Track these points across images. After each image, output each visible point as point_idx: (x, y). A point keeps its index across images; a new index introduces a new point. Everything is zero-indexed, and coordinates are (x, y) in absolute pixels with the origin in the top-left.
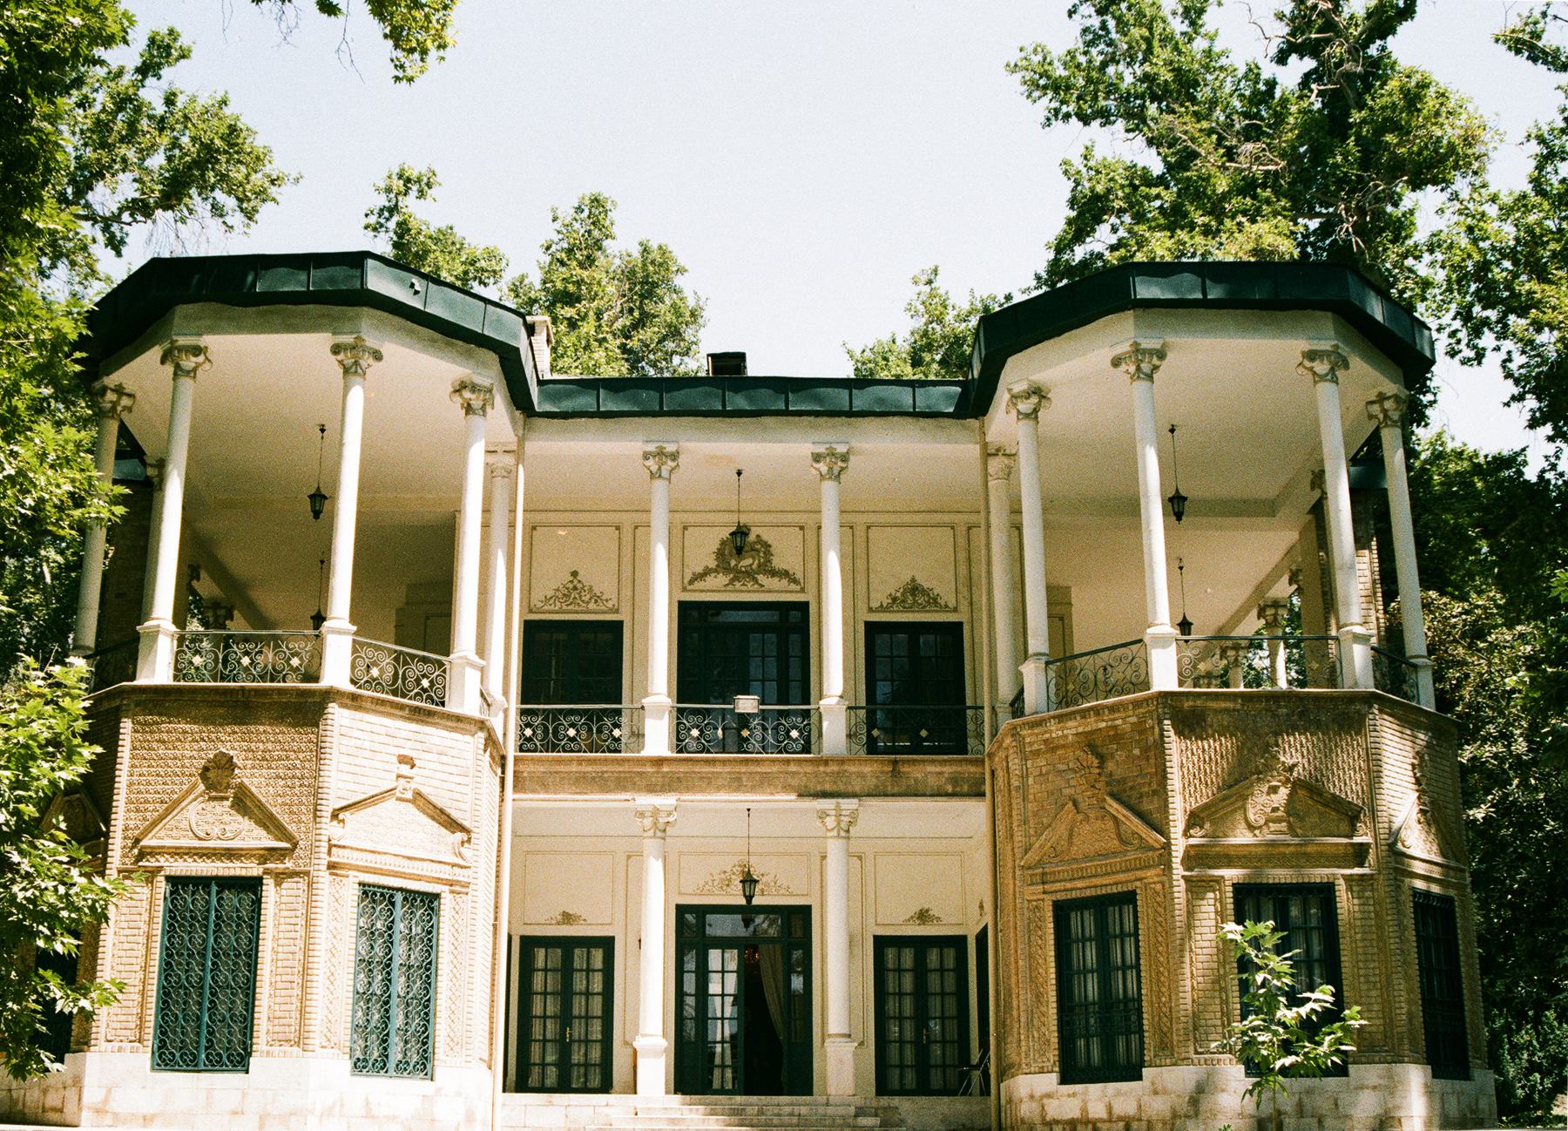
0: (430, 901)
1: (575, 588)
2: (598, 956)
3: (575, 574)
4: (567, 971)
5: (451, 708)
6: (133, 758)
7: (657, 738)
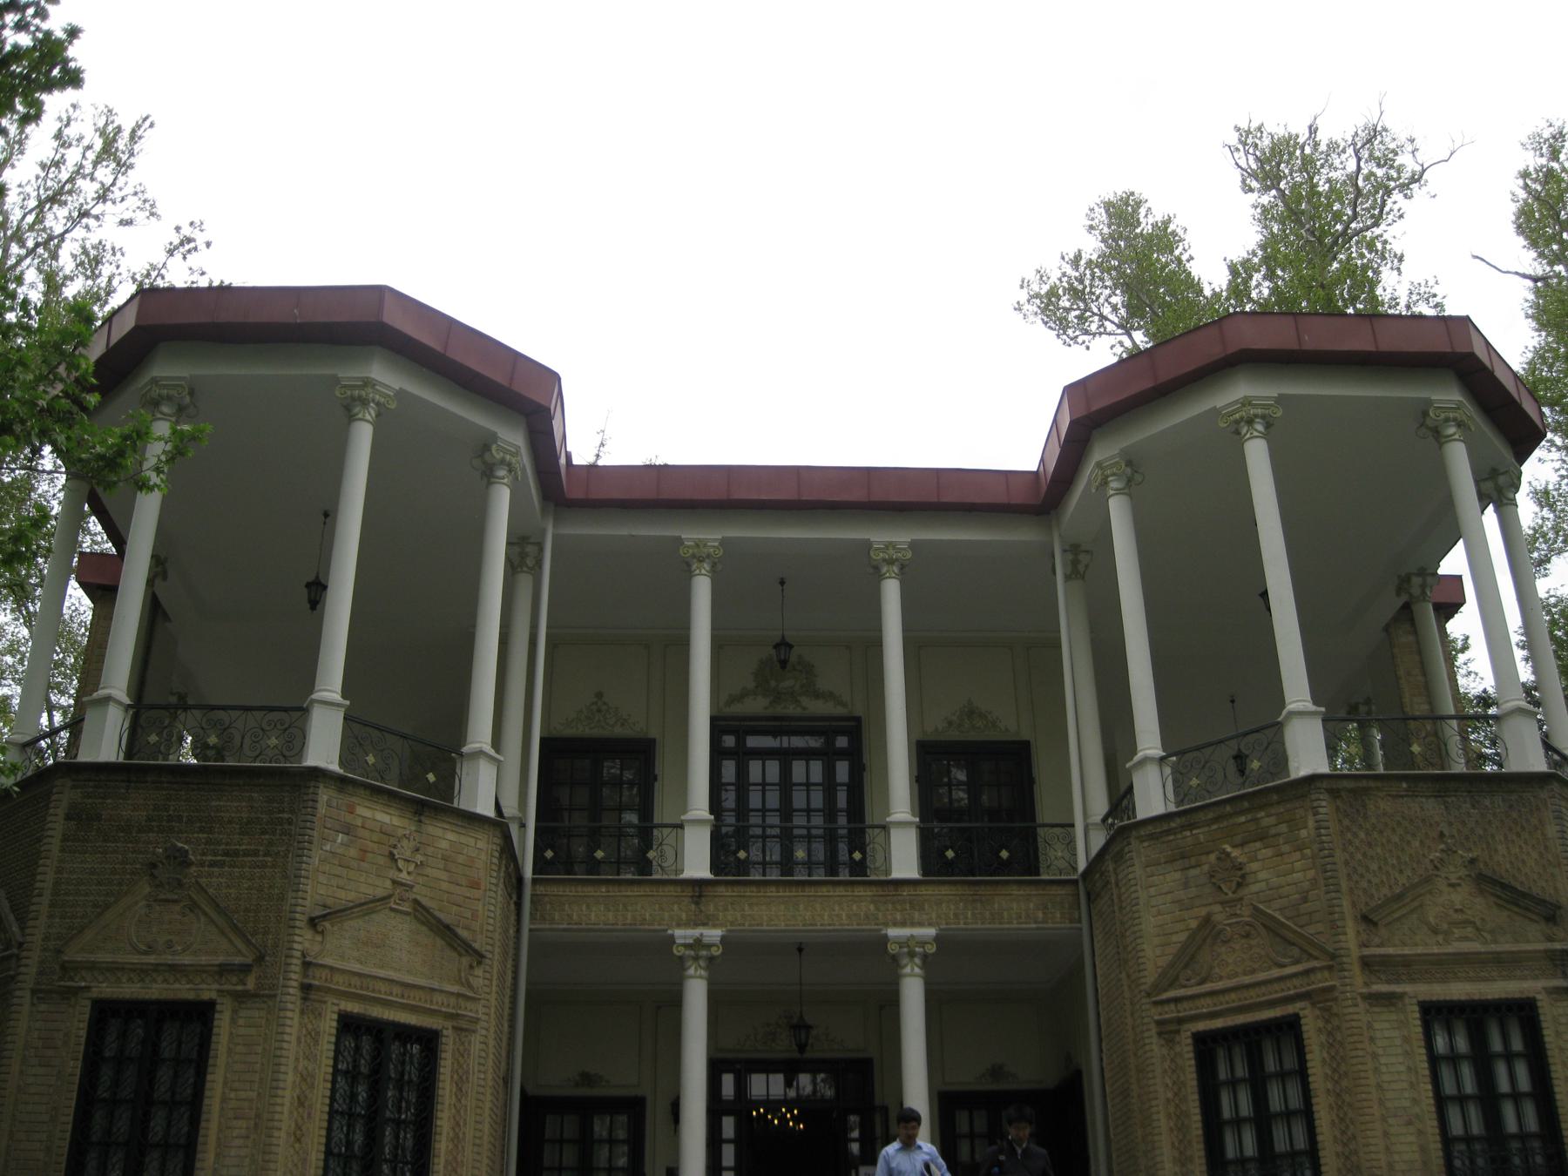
0: (429, 1041)
1: (599, 711)
3: (599, 695)
5: (463, 803)
6: (62, 850)
7: (696, 861)
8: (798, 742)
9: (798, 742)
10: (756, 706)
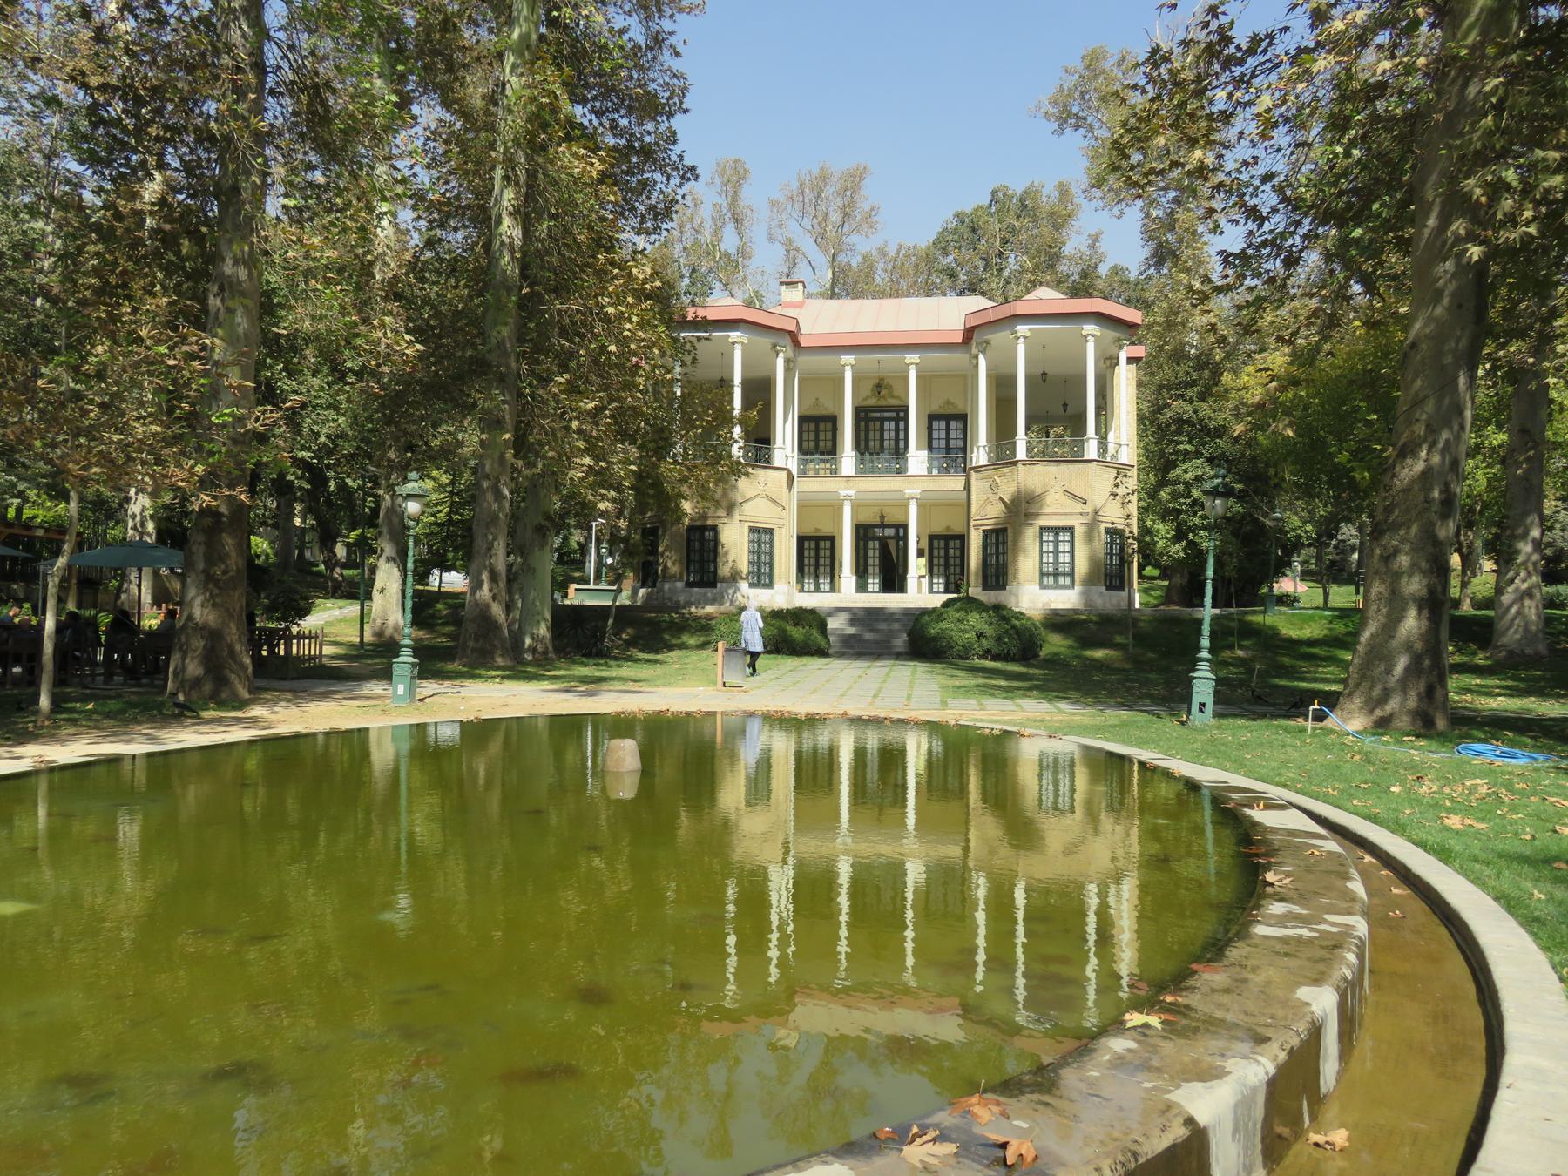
2: (828, 544)
4: (817, 548)
8: (887, 415)
9: (887, 415)
10: (872, 402)
